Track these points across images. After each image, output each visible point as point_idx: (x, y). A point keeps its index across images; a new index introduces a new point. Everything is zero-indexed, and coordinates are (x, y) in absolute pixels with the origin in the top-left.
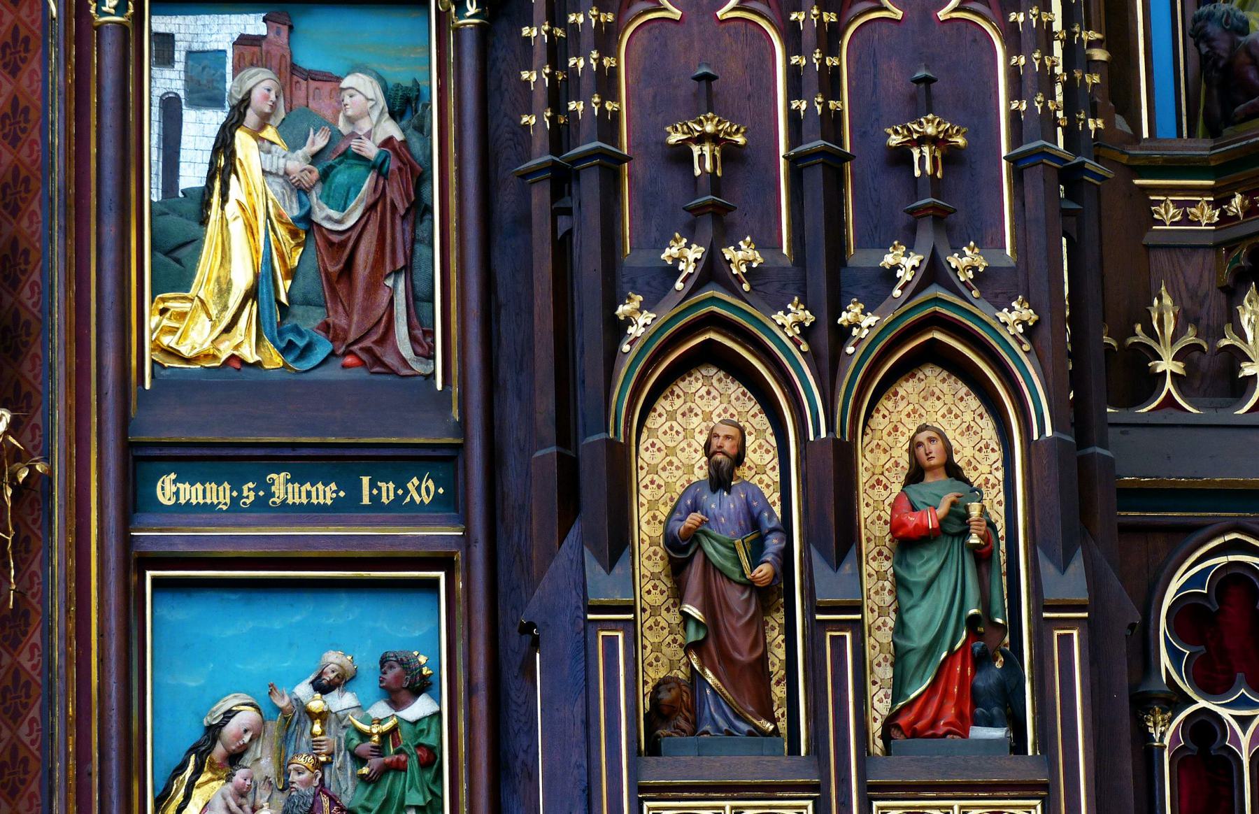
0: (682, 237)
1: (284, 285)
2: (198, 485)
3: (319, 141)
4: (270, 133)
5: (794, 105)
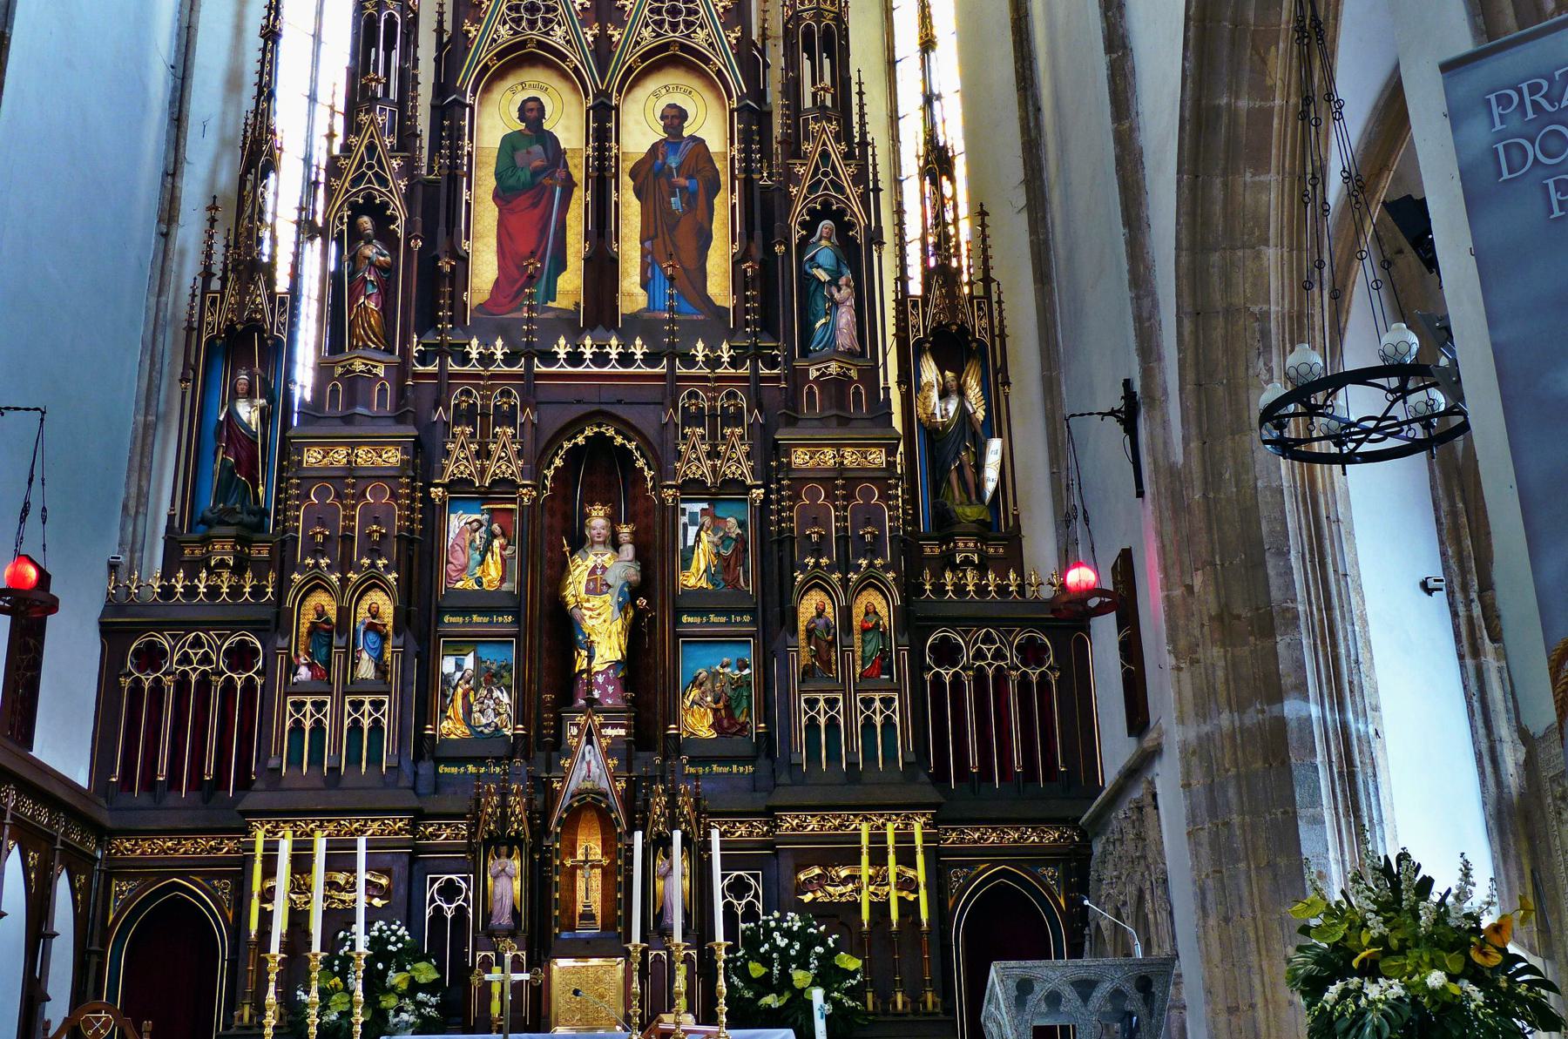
1: (713, 569)
4: (709, 532)
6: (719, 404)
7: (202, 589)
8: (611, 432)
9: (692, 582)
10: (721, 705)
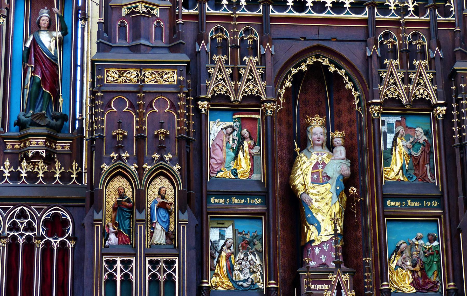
0: (114, 152)
1: (407, 166)
3: (412, 140)
4: (403, 138)
5: (178, 128)
6: (407, 42)
7: (24, 174)
8: (326, 62)
9: (392, 175)
10: (418, 268)
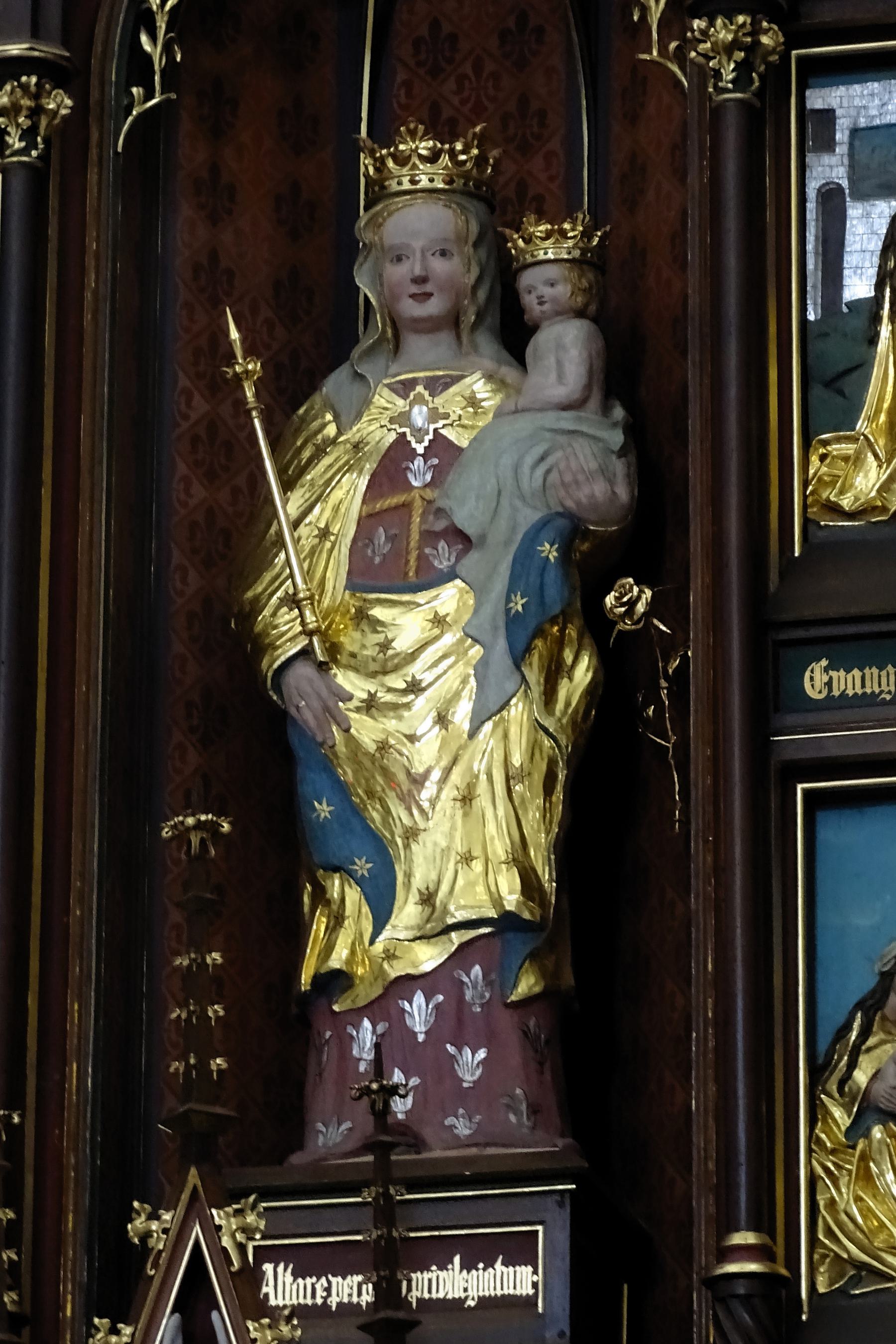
2: (856, 673)
